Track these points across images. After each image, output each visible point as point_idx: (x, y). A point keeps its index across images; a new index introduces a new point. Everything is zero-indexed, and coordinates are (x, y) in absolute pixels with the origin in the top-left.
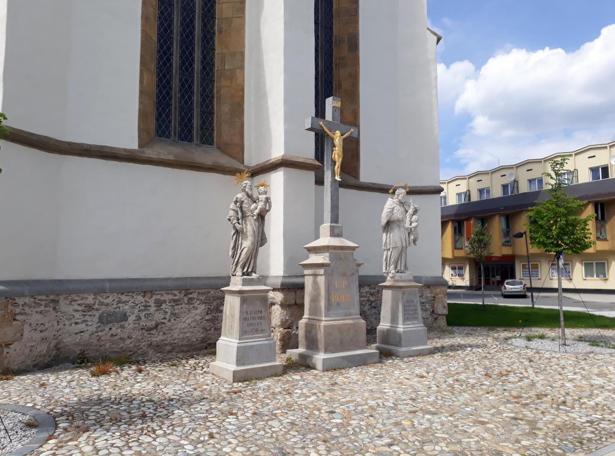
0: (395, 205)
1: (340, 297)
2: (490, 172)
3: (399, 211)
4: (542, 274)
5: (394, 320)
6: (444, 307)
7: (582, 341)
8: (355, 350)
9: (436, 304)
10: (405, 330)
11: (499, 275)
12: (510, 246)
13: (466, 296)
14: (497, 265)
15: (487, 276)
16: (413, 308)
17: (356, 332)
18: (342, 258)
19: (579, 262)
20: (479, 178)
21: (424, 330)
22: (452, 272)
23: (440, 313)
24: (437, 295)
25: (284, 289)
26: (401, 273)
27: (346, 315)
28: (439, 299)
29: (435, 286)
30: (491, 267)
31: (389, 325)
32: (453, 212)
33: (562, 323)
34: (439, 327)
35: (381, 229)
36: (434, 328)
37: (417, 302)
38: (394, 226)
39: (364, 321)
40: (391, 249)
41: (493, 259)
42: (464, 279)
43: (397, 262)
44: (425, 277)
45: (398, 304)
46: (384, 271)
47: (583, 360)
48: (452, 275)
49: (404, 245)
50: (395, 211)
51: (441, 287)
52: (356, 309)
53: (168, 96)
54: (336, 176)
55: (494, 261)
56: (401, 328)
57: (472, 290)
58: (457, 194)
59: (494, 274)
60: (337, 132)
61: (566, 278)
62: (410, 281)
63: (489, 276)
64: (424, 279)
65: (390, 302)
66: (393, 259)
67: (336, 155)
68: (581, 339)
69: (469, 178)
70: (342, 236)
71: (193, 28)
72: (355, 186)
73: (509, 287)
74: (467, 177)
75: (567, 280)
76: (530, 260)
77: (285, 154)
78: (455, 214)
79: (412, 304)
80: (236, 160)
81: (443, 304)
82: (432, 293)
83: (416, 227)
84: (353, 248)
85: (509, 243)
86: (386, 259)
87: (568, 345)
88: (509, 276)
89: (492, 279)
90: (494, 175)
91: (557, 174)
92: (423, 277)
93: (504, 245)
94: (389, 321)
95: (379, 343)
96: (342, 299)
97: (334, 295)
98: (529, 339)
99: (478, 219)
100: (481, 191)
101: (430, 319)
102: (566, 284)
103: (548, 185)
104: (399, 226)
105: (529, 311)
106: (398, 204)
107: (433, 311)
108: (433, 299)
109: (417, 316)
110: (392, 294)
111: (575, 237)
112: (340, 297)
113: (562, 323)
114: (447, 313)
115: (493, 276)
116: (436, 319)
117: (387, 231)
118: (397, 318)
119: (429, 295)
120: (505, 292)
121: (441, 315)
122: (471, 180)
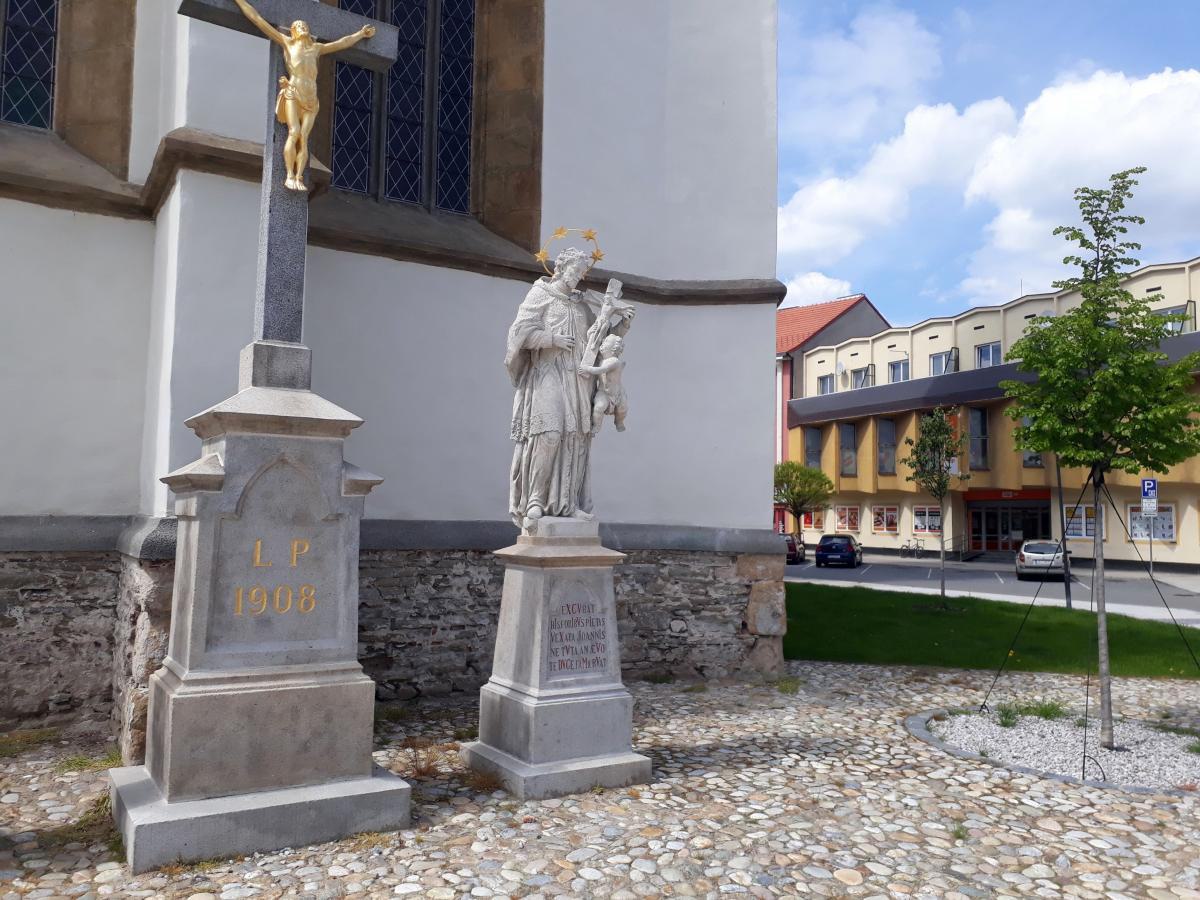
0: (551, 299)
1: (271, 597)
2: (1001, 309)
3: (561, 317)
4: (1110, 526)
5: (521, 670)
6: (775, 615)
7: (1165, 729)
8: (321, 782)
9: (752, 605)
10: (545, 703)
11: (1018, 529)
12: (1041, 467)
13: (941, 576)
14: (1013, 508)
15: (992, 531)
16: (588, 629)
17: (328, 718)
18: (291, 459)
19: (1193, 505)
20: (978, 321)
21: (624, 702)
22: (916, 521)
23: (762, 631)
24: (757, 581)
25: (158, 561)
26: (560, 515)
27: (290, 660)
28: (760, 591)
29: (750, 555)
30: (1000, 512)
31: (509, 682)
32: (921, 394)
33: (1104, 667)
34: (759, 670)
35: (508, 379)
36: (746, 673)
37: (604, 611)
38: (544, 367)
39: (366, 681)
40: (530, 440)
41: (1004, 495)
42: (859, 533)
43: (549, 482)
44: (725, 530)
45: (533, 617)
46: (512, 509)
47: (1149, 833)
48: (916, 527)
49: (571, 426)
50: (549, 320)
51: (768, 558)
52: (344, 636)
53: (412, 181)
54: (290, 174)
55: (1005, 500)
56: (532, 700)
57: (958, 560)
58: (930, 356)
59: (1007, 527)
60: (295, 23)
61: (1163, 539)
62: (583, 542)
63: (995, 532)
64: (722, 534)
65: (518, 606)
66: (534, 473)
67: (289, 103)
68: (1166, 722)
69: (957, 322)
70: (308, 386)
71: (445, 39)
72: (521, 271)
73: (1033, 557)
74: (953, 320)
75: (1165, 543)
76: (1063, 500)
77: (187, 125)
78: (924, 398)
79: (584, 616)
80: (104, 166)
81: (772, 607)
82: (743, 575)
83: (611, 370)
84: (342, 428)
85: (1039, 462)
86: (518, 471)
87: (1120, 749)
88: (1040, 531)
89: (1002, 539)
90: (1011, 315)
91: (1100, 233)
92: (720, 530)
93: (1026, 465)
94: (511, 671)
95: (483, 741)
96: (283, 604)
97: (247, 593)
98: (1008, 718)
99: (972, 408)
100: (982, 350)
101: (735, 647)
102: (1163, 554)
103: (1071, 263)
104: (558, 367)
105: (1054, 619)
106: (558, 298)
107: (744, 625)
108: (745, 590)
109: (601, 655)
110: (526, 582)
111: (1150, 416)
112: (271, 597)
113: (1104, 667)
114: (784, 631)
115: (1005, 532)
116: (752, 647)
117: (526, 381)
118: (529, 663)
119: (735, 580)
120: (1021, 567)
121: (767, 636)
122: (961, 326)
